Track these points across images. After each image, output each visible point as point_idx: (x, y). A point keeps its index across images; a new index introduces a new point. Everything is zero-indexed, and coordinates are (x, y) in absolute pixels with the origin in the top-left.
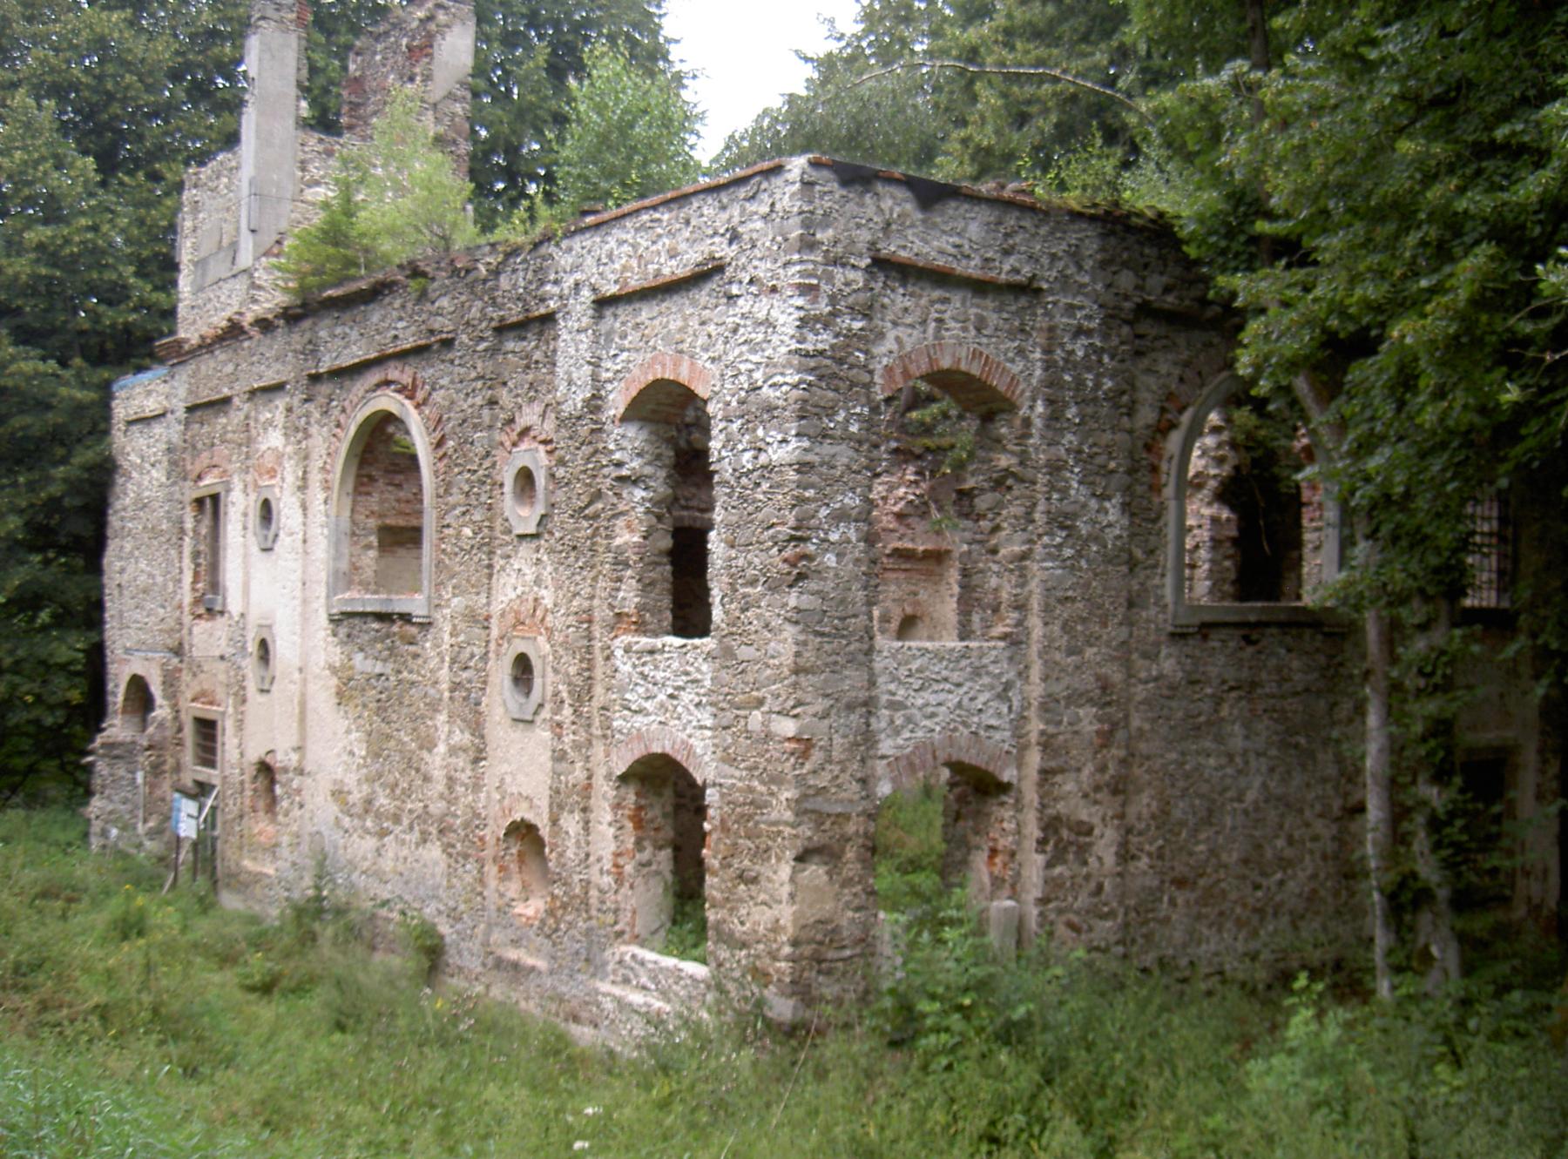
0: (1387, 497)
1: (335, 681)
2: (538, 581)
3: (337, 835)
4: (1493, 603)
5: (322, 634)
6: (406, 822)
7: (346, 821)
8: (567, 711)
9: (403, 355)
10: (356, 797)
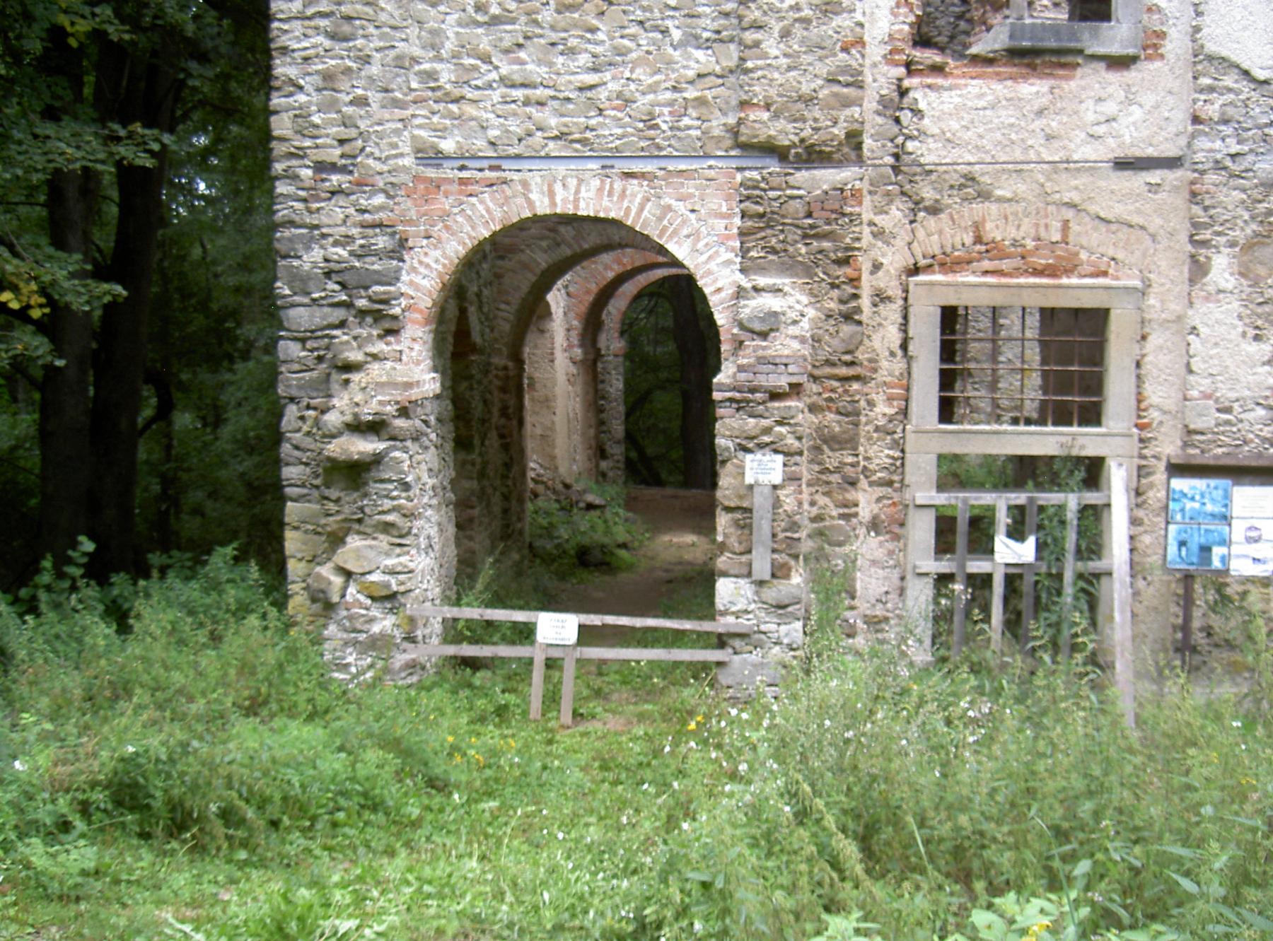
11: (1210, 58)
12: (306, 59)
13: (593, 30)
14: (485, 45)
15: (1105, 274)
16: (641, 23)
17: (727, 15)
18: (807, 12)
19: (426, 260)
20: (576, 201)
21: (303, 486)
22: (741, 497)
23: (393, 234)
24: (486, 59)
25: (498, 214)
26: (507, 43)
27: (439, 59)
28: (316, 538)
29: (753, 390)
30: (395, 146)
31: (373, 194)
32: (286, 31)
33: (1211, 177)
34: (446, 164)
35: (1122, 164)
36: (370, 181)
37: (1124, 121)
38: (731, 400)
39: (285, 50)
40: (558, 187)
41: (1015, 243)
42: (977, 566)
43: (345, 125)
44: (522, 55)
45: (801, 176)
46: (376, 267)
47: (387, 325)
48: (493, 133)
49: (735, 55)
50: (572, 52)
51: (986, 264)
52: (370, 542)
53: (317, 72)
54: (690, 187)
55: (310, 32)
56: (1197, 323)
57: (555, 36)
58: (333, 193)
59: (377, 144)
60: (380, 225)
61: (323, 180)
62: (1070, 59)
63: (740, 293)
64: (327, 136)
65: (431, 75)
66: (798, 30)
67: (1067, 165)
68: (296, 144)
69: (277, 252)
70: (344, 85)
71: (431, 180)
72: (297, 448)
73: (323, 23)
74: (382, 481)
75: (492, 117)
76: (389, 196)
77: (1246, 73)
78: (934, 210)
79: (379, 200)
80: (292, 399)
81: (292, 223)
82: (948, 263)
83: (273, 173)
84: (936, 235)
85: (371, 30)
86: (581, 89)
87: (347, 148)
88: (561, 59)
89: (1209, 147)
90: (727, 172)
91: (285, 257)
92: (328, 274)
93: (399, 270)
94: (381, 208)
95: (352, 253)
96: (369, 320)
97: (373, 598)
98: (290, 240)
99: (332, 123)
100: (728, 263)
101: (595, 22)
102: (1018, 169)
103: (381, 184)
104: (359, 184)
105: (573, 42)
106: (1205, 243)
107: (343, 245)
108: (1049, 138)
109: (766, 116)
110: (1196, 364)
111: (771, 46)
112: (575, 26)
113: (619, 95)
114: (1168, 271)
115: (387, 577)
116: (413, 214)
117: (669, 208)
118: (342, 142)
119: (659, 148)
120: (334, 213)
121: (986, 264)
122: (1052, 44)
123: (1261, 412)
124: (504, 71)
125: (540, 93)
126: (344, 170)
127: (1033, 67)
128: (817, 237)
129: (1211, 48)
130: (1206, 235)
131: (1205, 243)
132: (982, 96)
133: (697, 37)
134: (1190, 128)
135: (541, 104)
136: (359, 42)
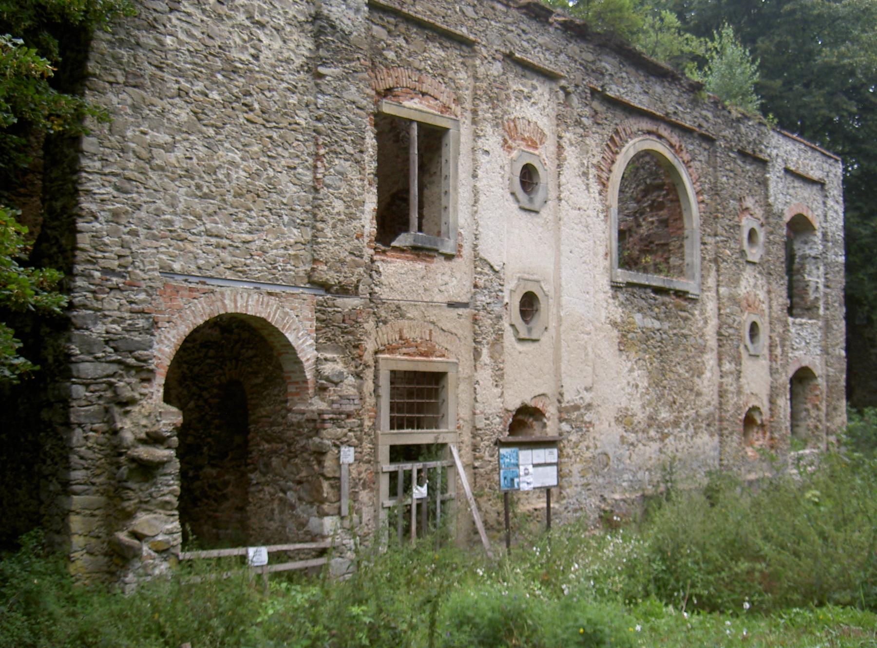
0: (596, 624)
1: (615, 333)
2: (755, 286)
3: (624, 451)
4: (251, 551)
5: (601, 296)
7: (632, 437)
10: (641, 417)
12: (102, 200)
13: (250, 210)
14: (199, 209)
15: (444, 356)
16: (270, 210)
17: (307, 212)
18: (343, 217)
19: (169, 336)
20: (247, 306)
21: (85, 484)
22: (335, 472)
23: (147, 319)
25: (208, 311)
26: (210, 211)
28: (92, 519)
29: (340, 413)
30: (152, 263)
32: (90, 180)
33: (482, 313)
34: (177, 277)
35: (452, 305)
36: (137, 283)
37: (451, 285)
38: (331, 419)
39: (88, 192)
40: (239, 298)
43: (122, 247)
44: (216, 218)
45: (339, 301)
46: (137, 339)
48: (201, 262)
49: (310, 233)
50: (240, 220)
51: (404, 350)
52: (152, 516)
53: (109, 210)
55: (106, 184)
56: (478, 378)
57: (232, 211)
58: (111, 289)
59: (142, 261)
60: (142, 312)
61: (107, 280)
62: (432, 254)
64: (112, 252)
65: (170, 223)
68: (92, 254)
69: (73, 324)
70: (124, 221)
71: (175, 287)
72: (82, 458)
73: (114, 179)
74: (165, 475)
77: (492, 267)
78: (385, 322)
79: (142, 296)
80: (80, 425)
81: (85, 307)
83: (75, 272)
84: (387, 334)
85: (142, 190)
86: (244, 242)
87: (123, 261)
90: (309, 297)
91: (78, 329)
92: (107, 342)
93: (151, 341)
94: (144, 301)
95: (124, 329)
96: (133, 372)
97: (156, 551)
98: (84, 317)
100: (311, 345)
102: (414, 304)
103: (144, 286)
104: (131, 285)
105: (241, 215)
108: (425, 290)
109: (325, 268)
112: (242, 206)
114: (466, 357)
115: (167, 537)
116: (163, 307)
117: (287, 314)
118: (120, 257)
119: (277, 280)
120: (112, 303)
121: (404, 350)
122: (428, 246)
123: (498, 419)
124: (208, 226)
125: (225, 242)
126: (120, 275)
127: (418, 255)
128: (347, 333)
129: (482, 255)
130: (480, 339)
131: (480, 343)
132: (402, 267)
133: (294, 222)
134: (473, 290)
135: (224, 248)
136: (135, 195)
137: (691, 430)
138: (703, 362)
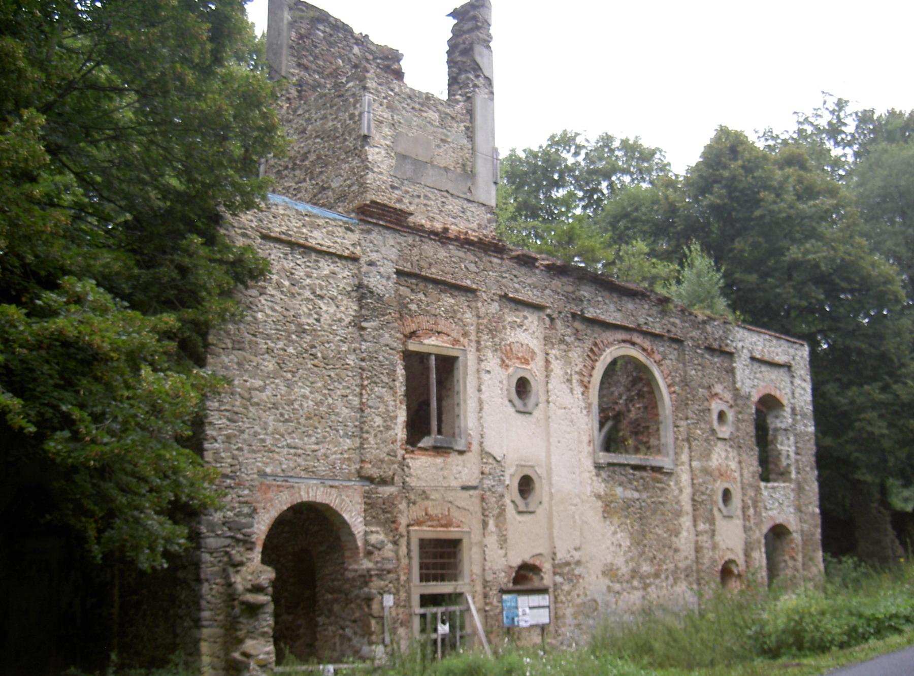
2: (727, 458)
5: (587, 475)
6: (663, 576)
7: (617, 587)
8: (751, 511)
9: (645, 334)
10: (624, 570)
11: (486, 453)
13: (316, 428)
14: (282, 430)
18: (382, 428)
24: (282, 436)
26: (290, 431)
27: (266, 434)
31: (244, 489)
35: (465, 488)
37: (463, 473)
39: (211, 423)
41: (436, 516)
42: (434, 636)
43: (233, 459)
44: (294, 435)
45: (381, 489)
47: (249, 546)
48: (284, 466)
50: (309, 436)
51: (429, 523)
54: (350, 492)
63: (366, 533)
65: (263, 441)
66: (379, 435)
67: (448, 488)
73: (227, 414)
75: (284, 461)
76: (250, 490)
79: (246, 492)
80: (207, 580)
82: (419, 523)
85: (245, 419)
87: (233, 468)
88: (306, 439)
89: (488, 483)
92: (224, 524)
94: (247, 495)
96: (241, 544)
99: (228, 457)
101: (317, 425)
105: (310, 432)
106: (487, 516)
107: (231, 511)
109: (370, 466)
110: (487, 557)
111: (372, 440)
113: (325, 455)
114: (476, 527)
117: (343, 500)
118: (232, 466)
121: (429, 523)
124: (289, 441)
125: (300, 451)
127: (438, 453)
129: (487, 449)
130: (487, 513)
135: (299, 456)
136: (240, 424)
137: (671, 580)
138: (680, 525)
